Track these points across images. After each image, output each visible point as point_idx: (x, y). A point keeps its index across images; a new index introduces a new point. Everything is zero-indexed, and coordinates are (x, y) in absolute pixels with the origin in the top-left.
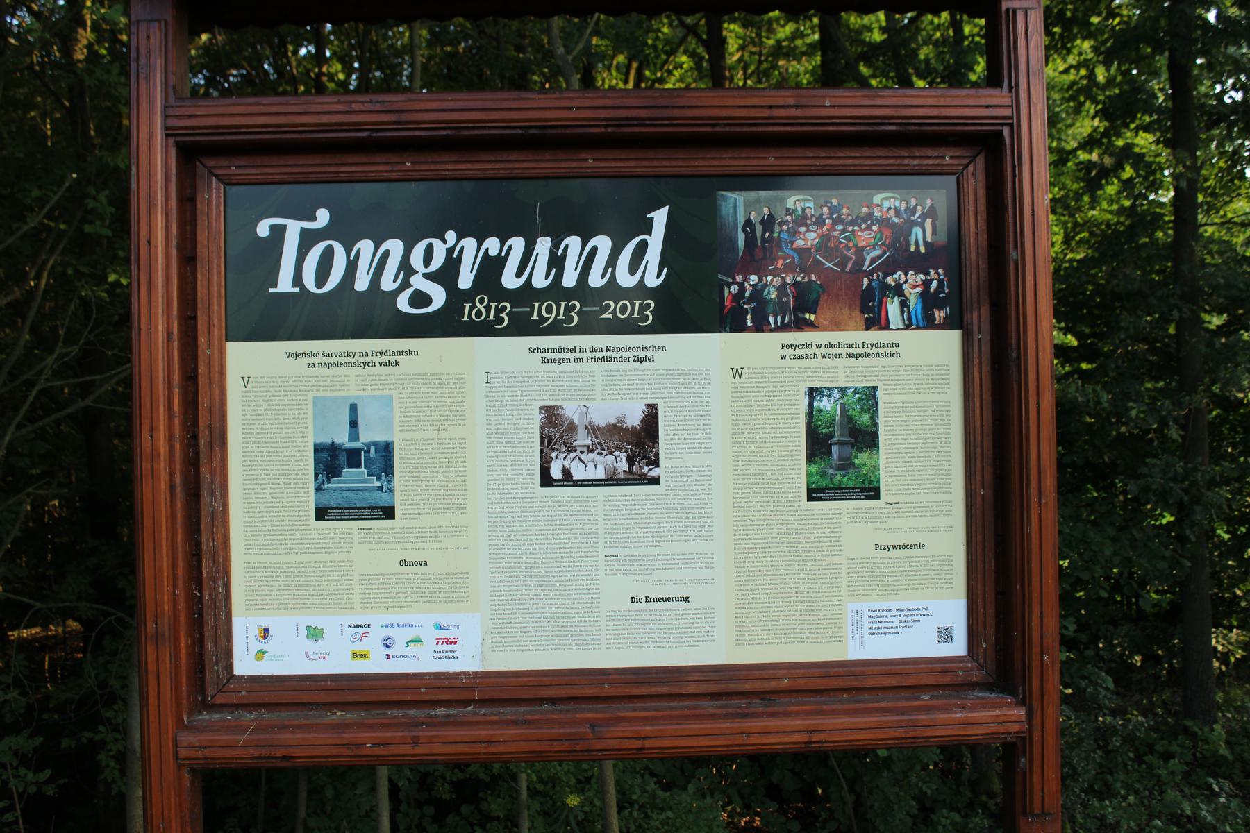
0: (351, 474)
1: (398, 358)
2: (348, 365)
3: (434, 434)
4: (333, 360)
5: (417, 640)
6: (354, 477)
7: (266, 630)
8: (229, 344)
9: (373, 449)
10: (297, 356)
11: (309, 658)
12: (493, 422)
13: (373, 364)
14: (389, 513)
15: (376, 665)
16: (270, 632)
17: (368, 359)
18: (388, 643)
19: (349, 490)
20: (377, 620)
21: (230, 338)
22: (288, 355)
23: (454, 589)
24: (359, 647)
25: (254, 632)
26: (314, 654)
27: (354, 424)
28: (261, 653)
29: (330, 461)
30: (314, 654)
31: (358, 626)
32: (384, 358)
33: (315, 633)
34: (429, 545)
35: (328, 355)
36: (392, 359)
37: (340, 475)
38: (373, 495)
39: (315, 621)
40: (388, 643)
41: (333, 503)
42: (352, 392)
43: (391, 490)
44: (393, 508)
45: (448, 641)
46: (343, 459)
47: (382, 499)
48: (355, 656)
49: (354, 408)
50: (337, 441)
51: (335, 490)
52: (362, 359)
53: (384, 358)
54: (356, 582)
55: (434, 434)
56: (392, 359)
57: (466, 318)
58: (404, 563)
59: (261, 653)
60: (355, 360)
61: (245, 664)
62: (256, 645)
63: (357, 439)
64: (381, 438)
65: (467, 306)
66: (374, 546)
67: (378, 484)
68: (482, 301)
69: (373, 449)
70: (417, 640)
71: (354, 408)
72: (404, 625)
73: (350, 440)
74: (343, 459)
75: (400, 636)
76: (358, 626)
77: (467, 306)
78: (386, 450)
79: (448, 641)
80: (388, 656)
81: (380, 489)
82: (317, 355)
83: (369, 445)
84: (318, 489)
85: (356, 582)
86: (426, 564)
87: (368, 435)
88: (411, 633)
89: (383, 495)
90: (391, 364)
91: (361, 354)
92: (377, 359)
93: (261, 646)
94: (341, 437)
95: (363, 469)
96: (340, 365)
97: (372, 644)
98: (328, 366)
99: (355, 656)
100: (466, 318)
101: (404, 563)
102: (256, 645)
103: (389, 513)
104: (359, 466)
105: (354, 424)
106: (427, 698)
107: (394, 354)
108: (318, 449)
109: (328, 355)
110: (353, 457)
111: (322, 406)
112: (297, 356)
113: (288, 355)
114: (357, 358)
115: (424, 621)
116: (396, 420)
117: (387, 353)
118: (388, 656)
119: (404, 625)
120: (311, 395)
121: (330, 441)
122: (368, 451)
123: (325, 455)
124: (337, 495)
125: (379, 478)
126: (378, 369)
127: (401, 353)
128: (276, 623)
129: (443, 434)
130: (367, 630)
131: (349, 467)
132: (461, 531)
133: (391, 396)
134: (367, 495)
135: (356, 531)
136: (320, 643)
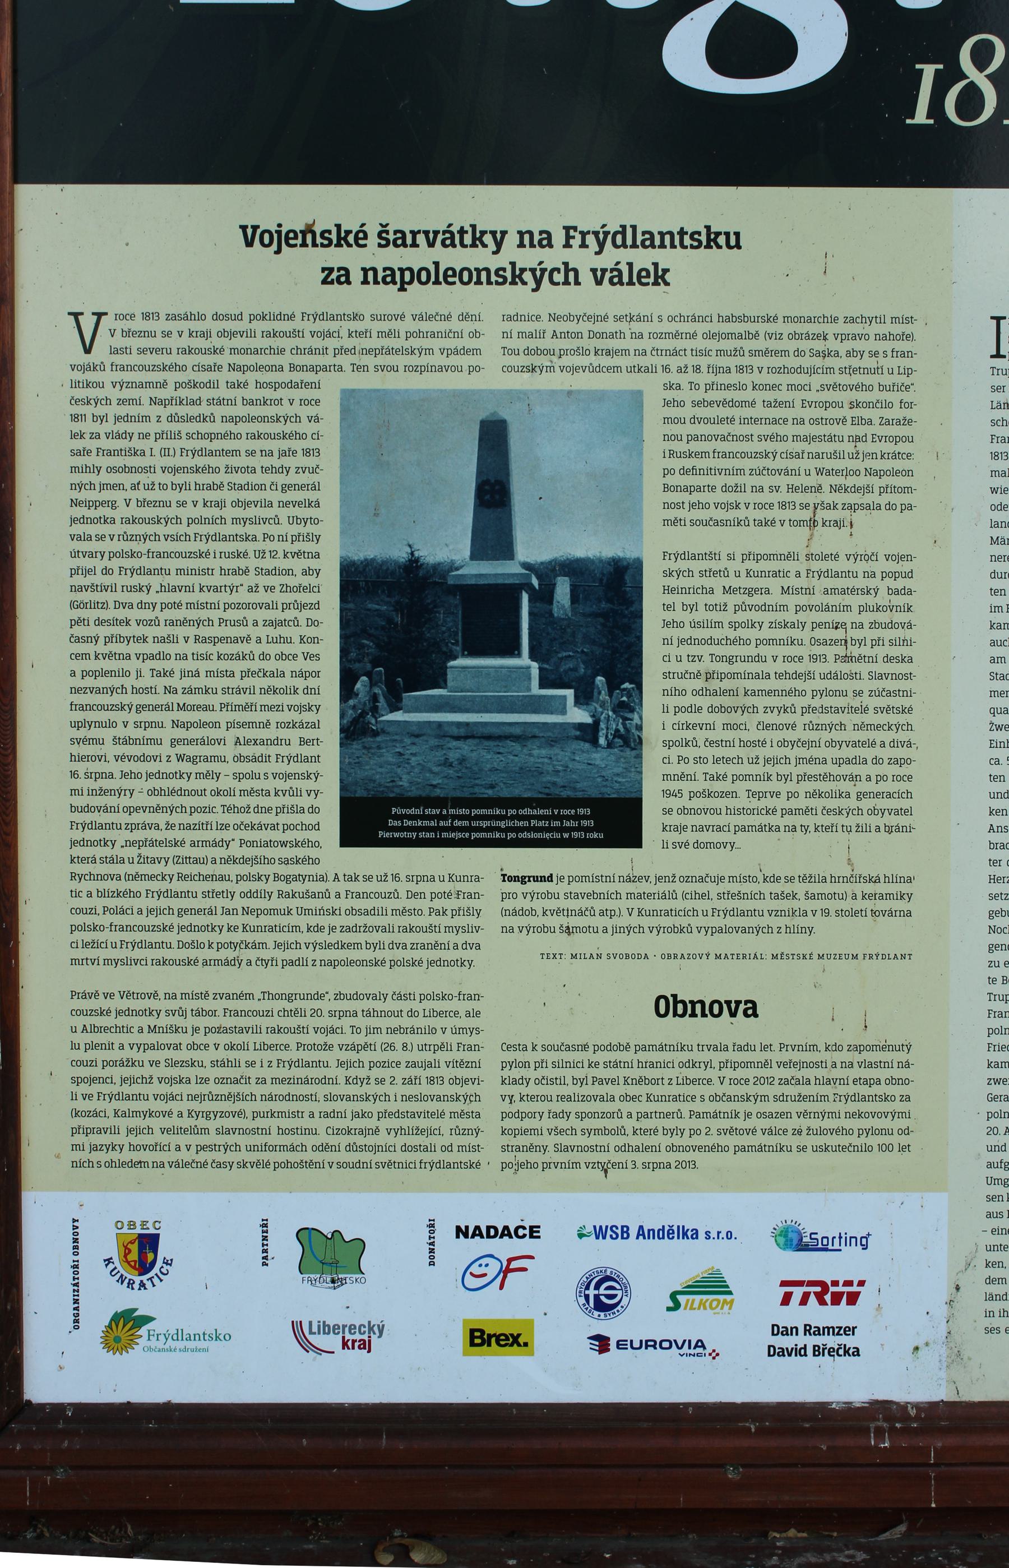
0: (485, 685)
1: (665, 257)
2: (475, 276)
3: (794, 540)
4: (420, 257)
5: (712, 1286)
6: (498, 690)
7: (149, 1242)
8: (16, 186)
9: (563, 590)
10: (281, 239)
11: (306, 1345)
12: (686, 395)
13: (570, 275)
14: (618, 822)
15: (558, 1372)
16: (164, 1250)
17: (553, 257)
18: (603, 1294)
19: (469, 733)
20: (563, 1209)
21: (16, 180)
22: (250, 235)
23: (854, 1103)
24: (493, 1308)
25: (102, 1243)
26: (326, 1329)
27: (493, 495)
28: (125, 1328)
29: (400, 625)
30: (326, 1329)
31: (492, 1232)
32: (611, 257)
33: (329, 1256)
34: (766, 944)
35: (402, 240)
36: (643, 258)
37: (438, 679)
38: (561, 755)
39: (334, 1210)
40: (603, 1294)
41: (406, 782)
42: (492, 376)
43: (630, 741)
44: (636, 804)
45: (825, 1292)
46: (449, 620)
47: (594, 768)
48: (479, 1338)
49: (494, 437)
50: (432, 554)
51: (416, 732)
52: (529, 258)
53: (611, 257)
54: (490, 1072)
55: (794, 540)
56: (643, 258)
57: (921, 116)
58: (669, 1006)
59: (125, 1328)
60: (502, 260)
61: (63, 1366)
62: (107, 1296)
63: (505, 549)
64: (591, 544)
65: (929, 71)
66: (559, 942)
67: (579, 716)
68: (982, 56)
69: (563, 590)
70: (712, 1286)
71: (494, 437)
72: (666, 1233)
73: (477, 554)
74: (449, 620)
75: (651, 1273)
76: (492, 1232)
77: (929, 71)
78: (612, 592)
79: (825, 1292)
80: (602, 1343)
81: (588, 733)
82: (360, 238)
83: (548, 572)
84: (354, 730)
85: (490, 1072)
86: (752, 1010)
87: (540, 539)
88: (688, 1261)
89: (598, 757)
90: (639, 278)
91: (525, 238)
92: (583, 259)
93: (125, 1299)
94: (447, 541)
95: (524, 660)
96: (447, 276)
97: (544, 1295)
98: (400, 279)
99: (479, 1338)
100: (921, 116)
101: (669, 1006)
102: (107, 1296)
103: (618, 822)
104: (512, 649)
105: (493, 495)
106: (749, 1499)
107: (649, 241)
108: (358, 581)
109: (402, 240)
110: (487, 616)
111: (373, 427)
112: (281, 239)
113: (250, 235)
114: (511, 250)
115: (740, 1216)
116: (652, 481)
117: (624, 237)
118: (602, 1343)
119: (666, 1233)
120: (331, 388)
121: (400, 554)
122: (544, 596)
123: (379, 606)
124: (420, 754)
125: (584, 698)
126: (587, 297)
127: (679, 239)
128: (192, 1216)
129: (827, 540)
130: (526, 1246)
131: (474, 650)
132: (887, 896)
133: (637, 398)
134: (538, 754)
135: (492, 887)
136: (350, 1291)
